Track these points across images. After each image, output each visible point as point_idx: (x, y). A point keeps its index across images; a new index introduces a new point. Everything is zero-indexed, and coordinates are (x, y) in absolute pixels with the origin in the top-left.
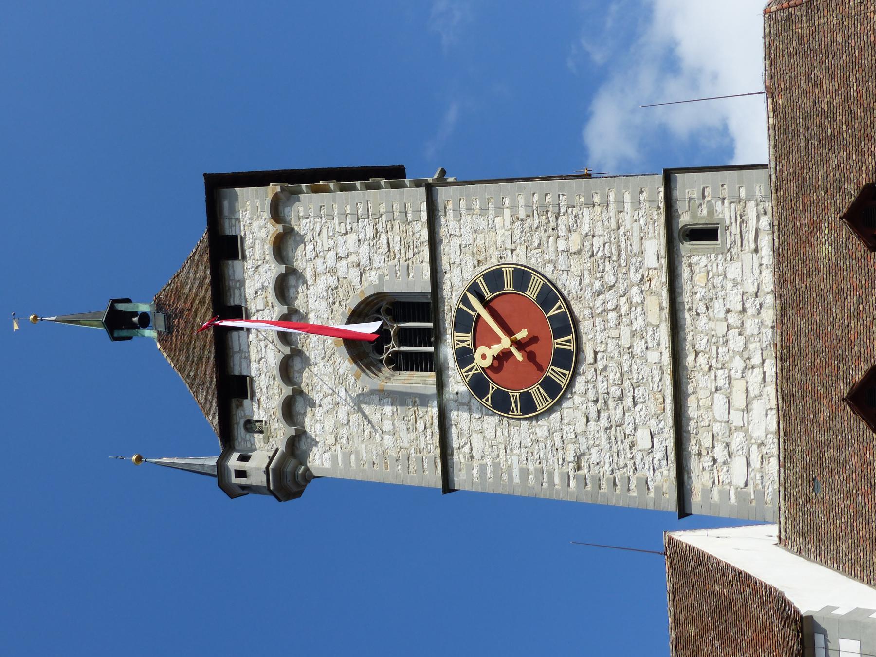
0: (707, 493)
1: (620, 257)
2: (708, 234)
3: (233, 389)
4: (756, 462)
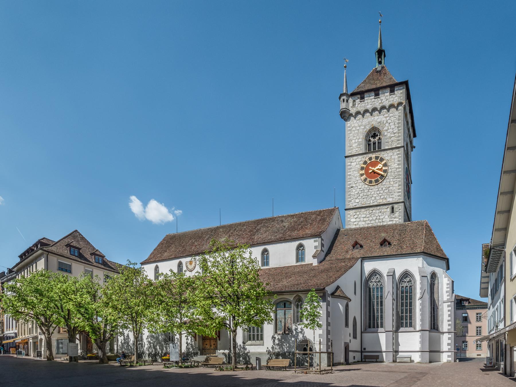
0: (349, 214)
1: (390, 193)
2: (393, 211)
3: (361, 94)
4: (355, 223)
